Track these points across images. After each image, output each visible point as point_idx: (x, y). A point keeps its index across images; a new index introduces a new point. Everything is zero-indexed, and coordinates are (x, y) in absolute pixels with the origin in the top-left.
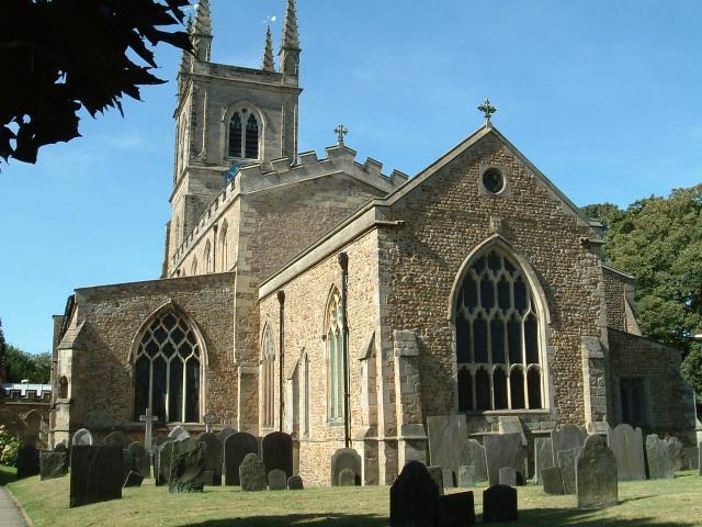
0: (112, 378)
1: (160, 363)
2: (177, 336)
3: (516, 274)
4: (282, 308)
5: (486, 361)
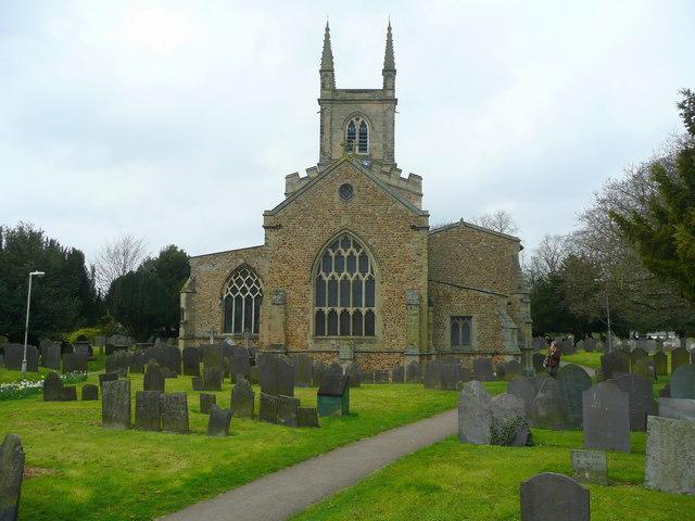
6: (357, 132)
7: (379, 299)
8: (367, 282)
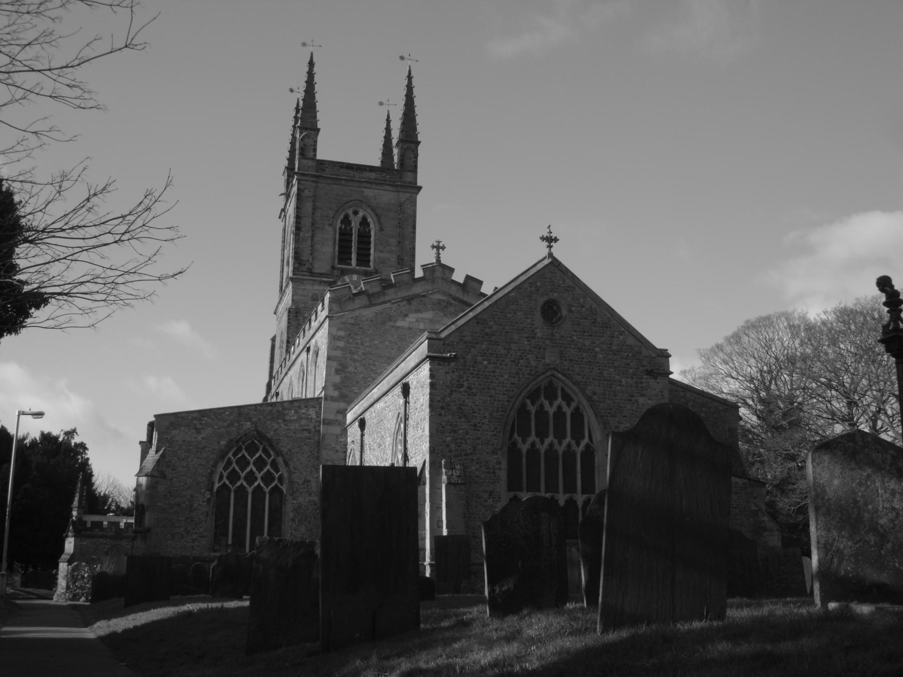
1: (241, 491)
2: (260, 464)
3: (573, 405)
4: (362, 435)
5: (521, 491)
8: (582, 454)
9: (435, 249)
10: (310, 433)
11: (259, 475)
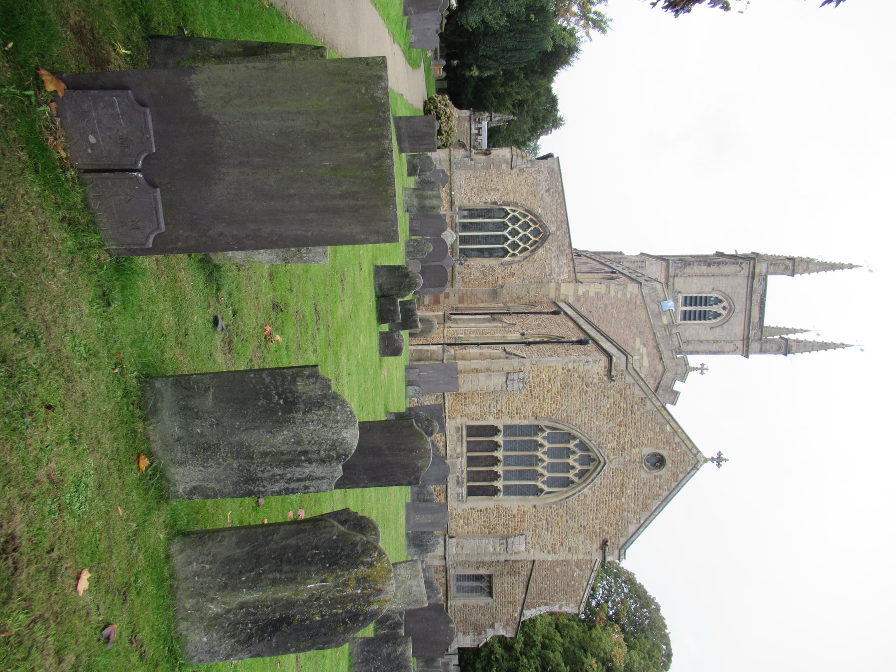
0: (491, 190)
1: (504, 226)
2: (525, 239)
4: (547, 313)
5: (505, 436)
6: (708, 308)
7: (513, 503)
9: (700, 367)
10: (549, 275)
11: (516, 239)
